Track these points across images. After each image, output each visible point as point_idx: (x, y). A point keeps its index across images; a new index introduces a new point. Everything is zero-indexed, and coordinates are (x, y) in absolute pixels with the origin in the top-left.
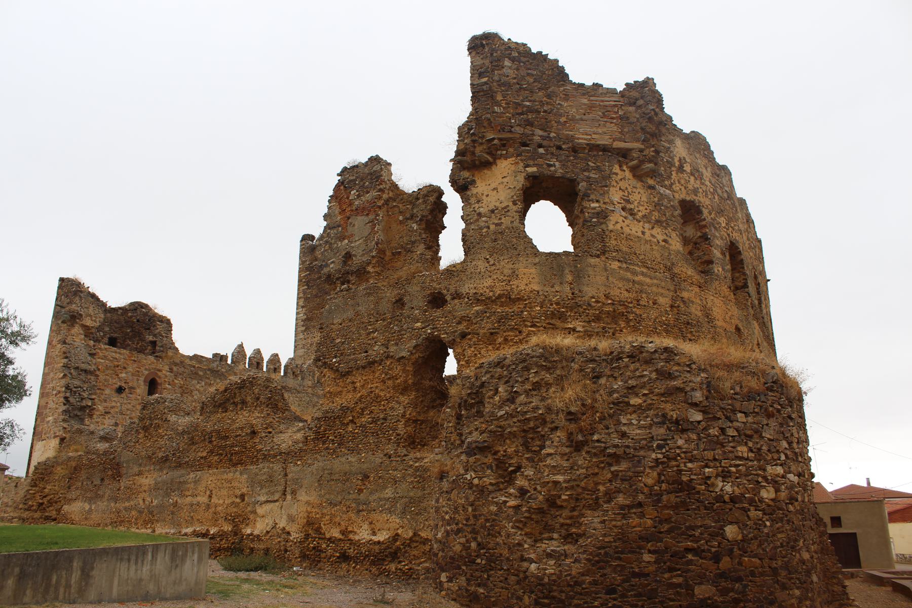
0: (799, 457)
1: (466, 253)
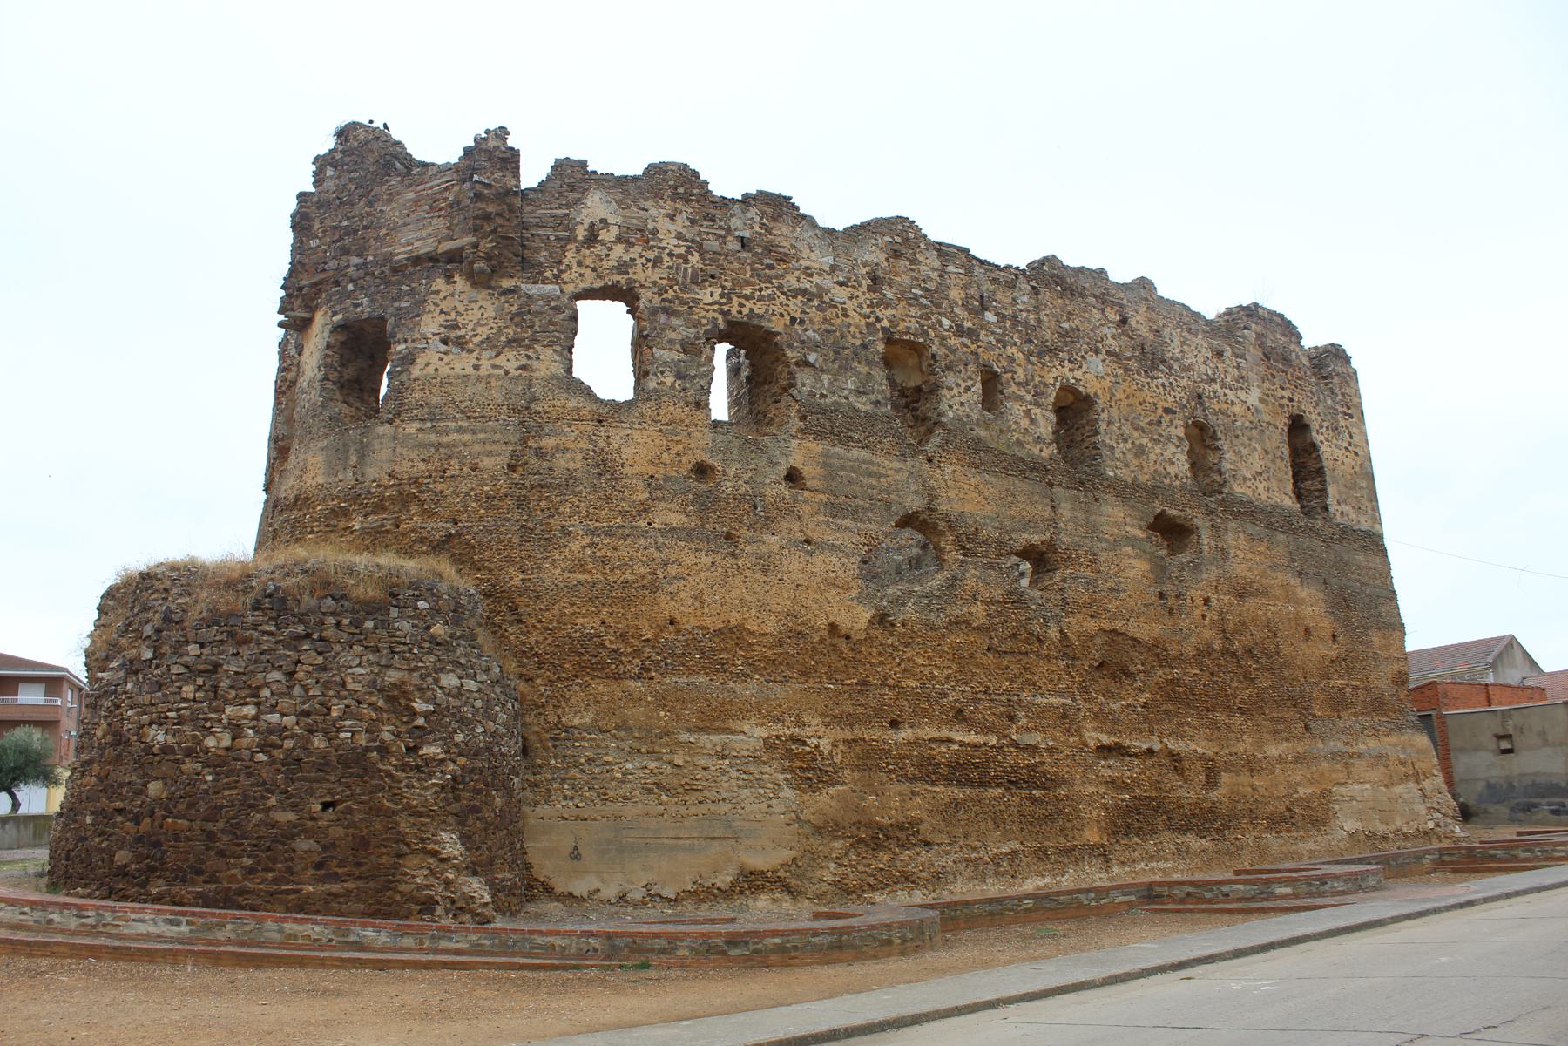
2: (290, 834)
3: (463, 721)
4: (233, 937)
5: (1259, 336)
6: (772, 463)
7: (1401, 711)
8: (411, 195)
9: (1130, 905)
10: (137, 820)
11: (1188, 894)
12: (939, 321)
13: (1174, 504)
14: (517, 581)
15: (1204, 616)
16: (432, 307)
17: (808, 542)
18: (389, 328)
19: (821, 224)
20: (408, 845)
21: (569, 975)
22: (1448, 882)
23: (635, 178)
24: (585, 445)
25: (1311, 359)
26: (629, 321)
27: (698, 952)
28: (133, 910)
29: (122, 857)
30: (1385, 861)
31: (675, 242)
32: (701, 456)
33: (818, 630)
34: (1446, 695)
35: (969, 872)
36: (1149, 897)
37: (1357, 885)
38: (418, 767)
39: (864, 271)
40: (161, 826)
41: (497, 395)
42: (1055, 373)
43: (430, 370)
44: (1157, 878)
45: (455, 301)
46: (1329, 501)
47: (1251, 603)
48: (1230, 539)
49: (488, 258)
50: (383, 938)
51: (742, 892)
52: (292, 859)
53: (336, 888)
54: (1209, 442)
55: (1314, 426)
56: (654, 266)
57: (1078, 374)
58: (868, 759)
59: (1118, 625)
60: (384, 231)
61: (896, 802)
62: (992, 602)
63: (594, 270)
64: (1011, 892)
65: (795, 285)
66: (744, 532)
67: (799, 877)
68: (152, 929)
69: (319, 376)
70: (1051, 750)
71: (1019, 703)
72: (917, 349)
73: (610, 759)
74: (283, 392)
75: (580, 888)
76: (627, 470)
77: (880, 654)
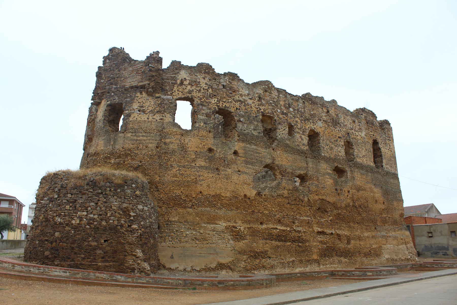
0: (403, 205)
1: (193, 125)
2: (95, 249)
3: (143, 218)
4: (81, 277)
5: (365, 117)
6: (230, 149)
7: (402, 224)
8: (131, 69)
9: (327, 277)
10: (52, 243)
11: (343, 274)
12: (277, 110)
13: (340, 164)
14: (158, 179)
15: (348, 196)
16: (136, 101)
17: (239, 171)
18: (123, 106)
19: (245, 82)
20: (128, 253)
21: (174, 290)
22: (414, 273)
23: (194, 67)
24: (178, 142)
25: (379, 124)
26: (191, 107)
27: (210, 285)
28: (54, 268)
29: (47, 253)
30: (397, 266)
31: (205, 85)
32: (210, 146)
33: (241, 196)
34: (414, 220)
35: (281, 266)
36: (332, 274)
37: (390, 273)
38: (131, 231)
39: (257, 95)
40: (58, 245)
41: (154, 126)
42: (309, 126)
43: (135, 119)
44: (333, 269)
45: (143, 100)
46: (383, 164)
47: (361, 192)
48: (356, 174)
49: (153, 88)
50: (123, 279)
51: (218, 269)
52: (95, 256)
53: (107, 264)
54: (350, 147)
55: (380, 143)
56: (199, 92)
57: (315, 126)
58: (254, 233)
59: (324, 197)
60: (123, 79)
61: (261, 245)
62: (290, 190)
63: (182, 92)
64: (292, 272)
65: (238, 99)
66: (221, 168)
67: (234, 266)
68: (59, 274)
69: (103, 119)
70: (304, 232)
71: (296, 218)
72: (271, 118)
73: (182, 230)
74: (90, 122)
75: (173, 266)
76: (190, 149)
77: (258, 203)
